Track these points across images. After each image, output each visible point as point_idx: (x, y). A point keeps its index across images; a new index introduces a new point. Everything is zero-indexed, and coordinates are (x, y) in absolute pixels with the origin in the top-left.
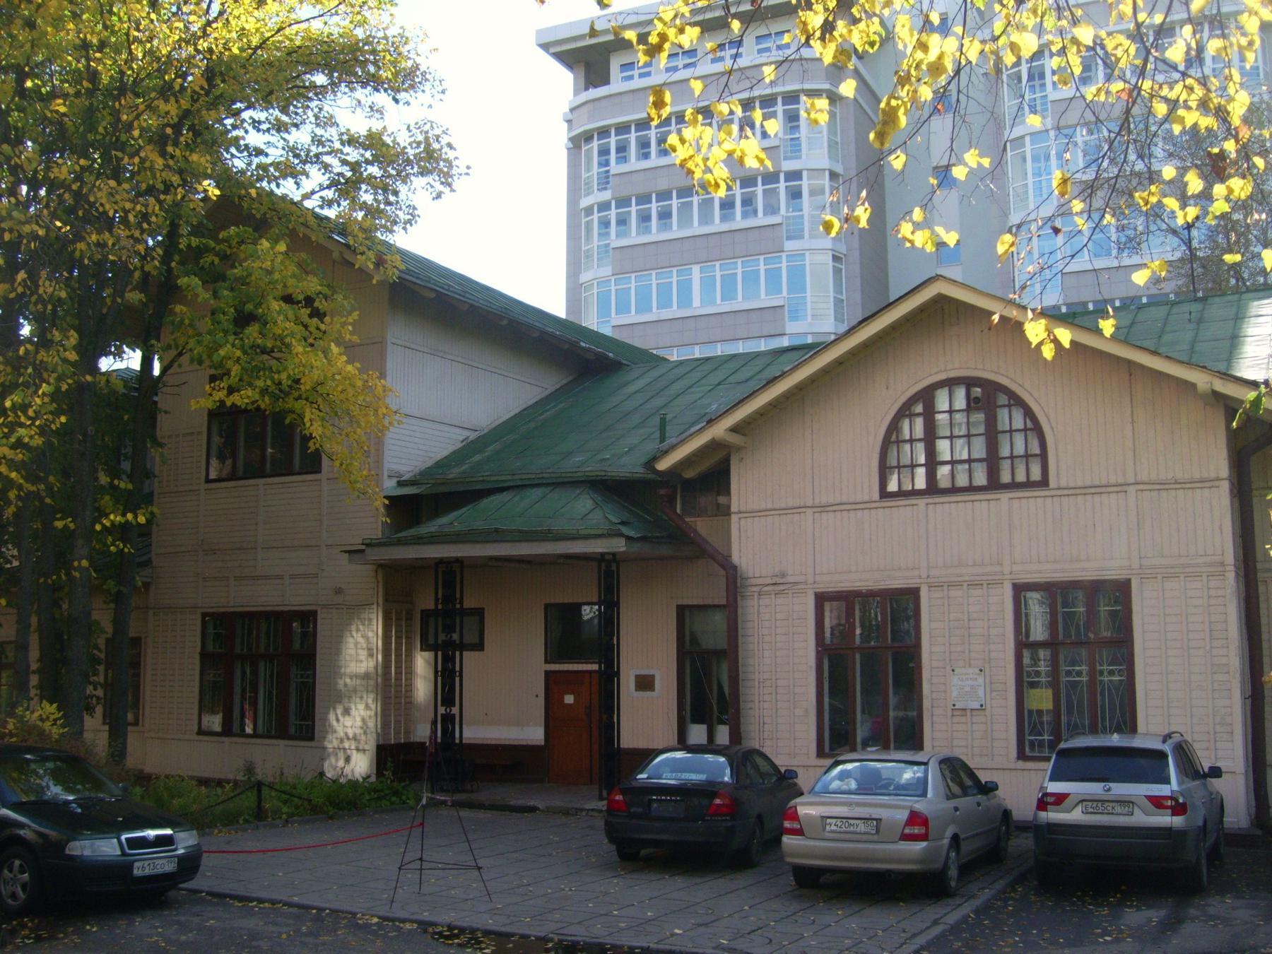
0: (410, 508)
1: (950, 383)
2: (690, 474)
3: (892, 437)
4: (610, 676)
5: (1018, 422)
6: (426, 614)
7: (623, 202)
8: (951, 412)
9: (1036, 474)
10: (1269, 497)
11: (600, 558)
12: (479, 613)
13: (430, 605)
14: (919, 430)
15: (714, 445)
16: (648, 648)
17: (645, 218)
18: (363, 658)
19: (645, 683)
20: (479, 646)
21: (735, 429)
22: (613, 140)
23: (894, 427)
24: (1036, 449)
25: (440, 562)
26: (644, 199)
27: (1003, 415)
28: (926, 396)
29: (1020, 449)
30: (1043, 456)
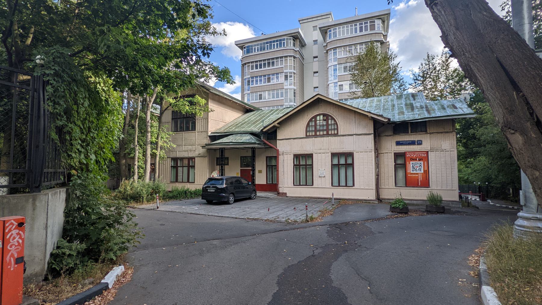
0: (214, 138)
1: (319, 115)
2: (269, 132)
3: (308, 125)
4: (254, 170)
5: (333, 122)
6: (217, 158)
7: (252, 77)
8: (320, 120)
9: (336, 132)
10: (489, 293)
11: (252, 148)
12: (228, 158)
13: (218, 156)
14: (313, 124)
15: (274, 126)
16: (261, 166)
17: (257, 81)
18: (125, 217)
19: (260, 172)
20: (228, 164)
21: (278, 124)
22: (254, 64)
23: (308, 124)
24: (336, 127)
25: (220, 148)
26: (256, 77)
27: (330, 121)
28: (315, 117)
29: (333, 128)
30: (337, 124)
